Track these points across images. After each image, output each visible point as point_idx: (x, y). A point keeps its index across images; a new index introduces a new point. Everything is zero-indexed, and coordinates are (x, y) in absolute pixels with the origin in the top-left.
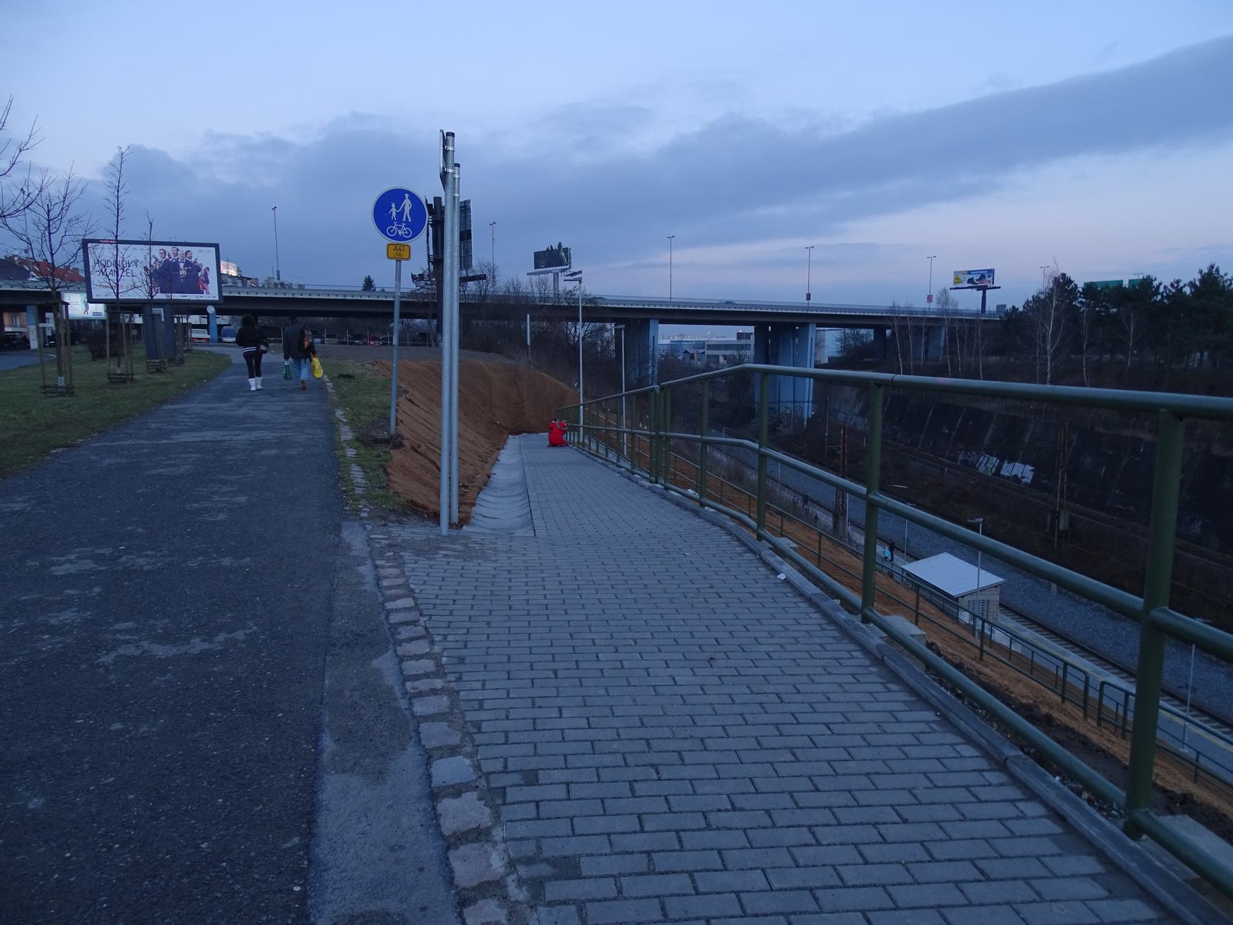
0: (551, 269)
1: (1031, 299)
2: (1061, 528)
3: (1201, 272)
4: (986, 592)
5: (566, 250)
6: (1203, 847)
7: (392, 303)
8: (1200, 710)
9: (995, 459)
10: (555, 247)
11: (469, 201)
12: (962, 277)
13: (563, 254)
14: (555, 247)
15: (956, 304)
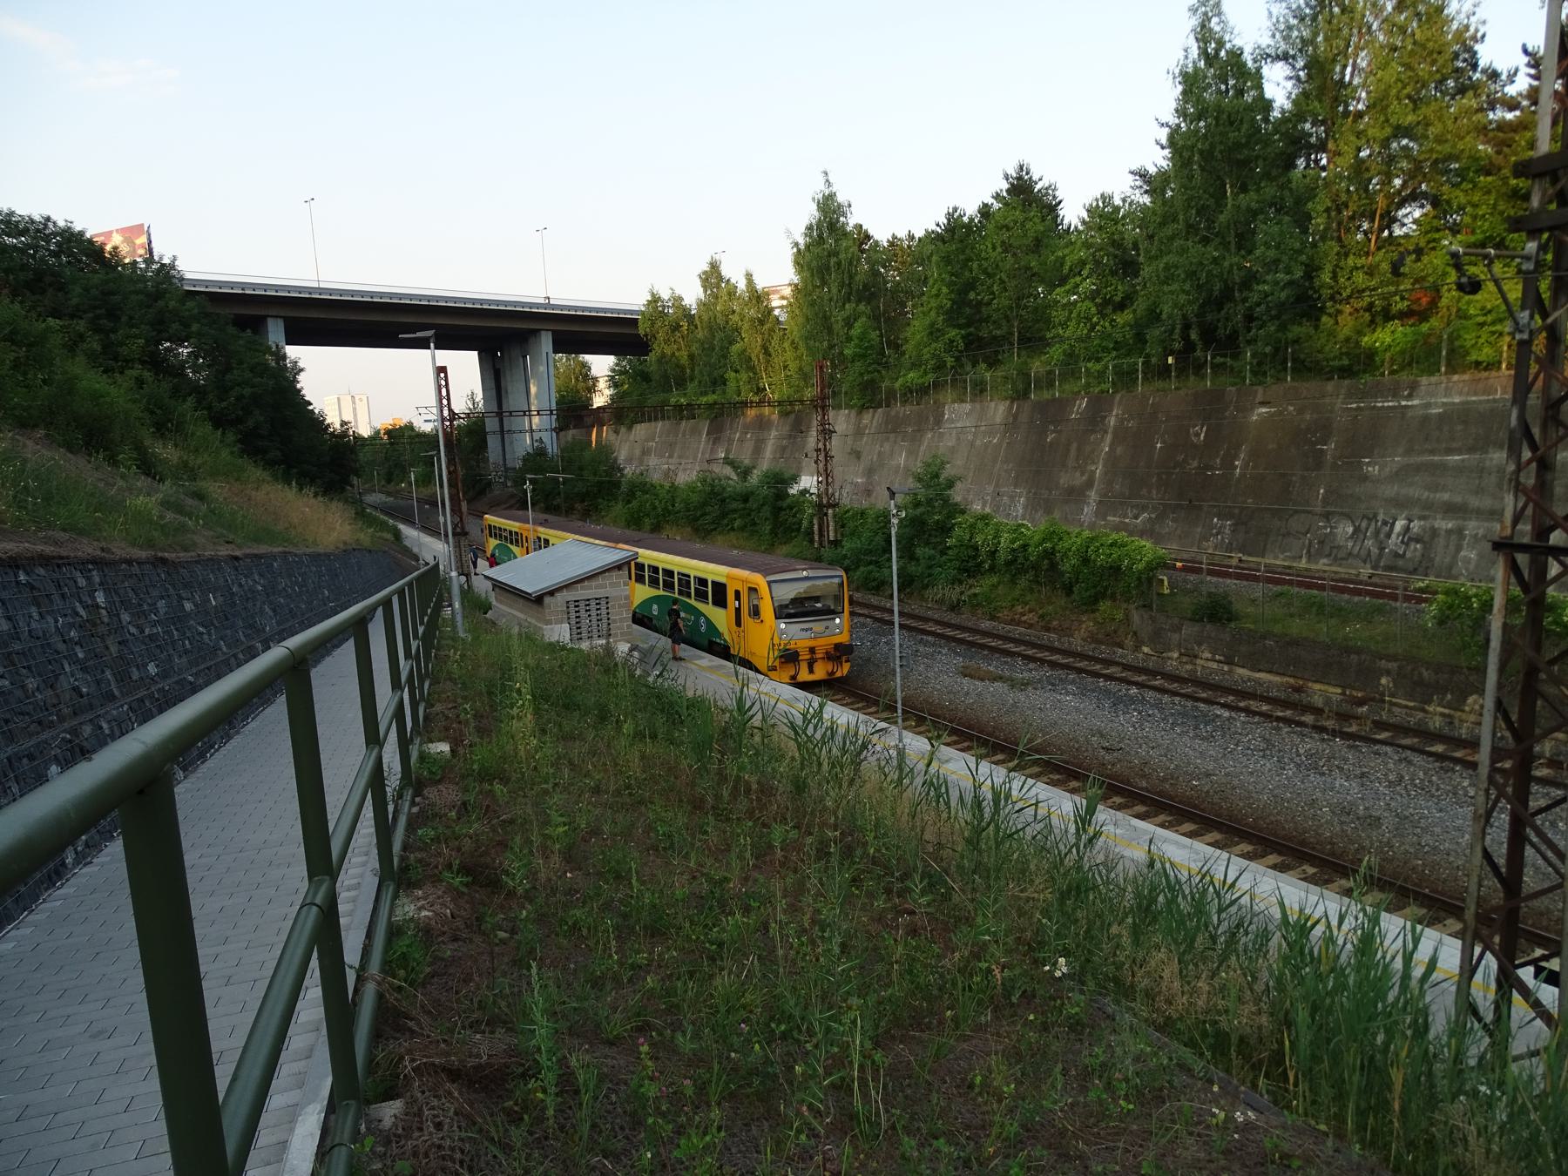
4: (600, 580)
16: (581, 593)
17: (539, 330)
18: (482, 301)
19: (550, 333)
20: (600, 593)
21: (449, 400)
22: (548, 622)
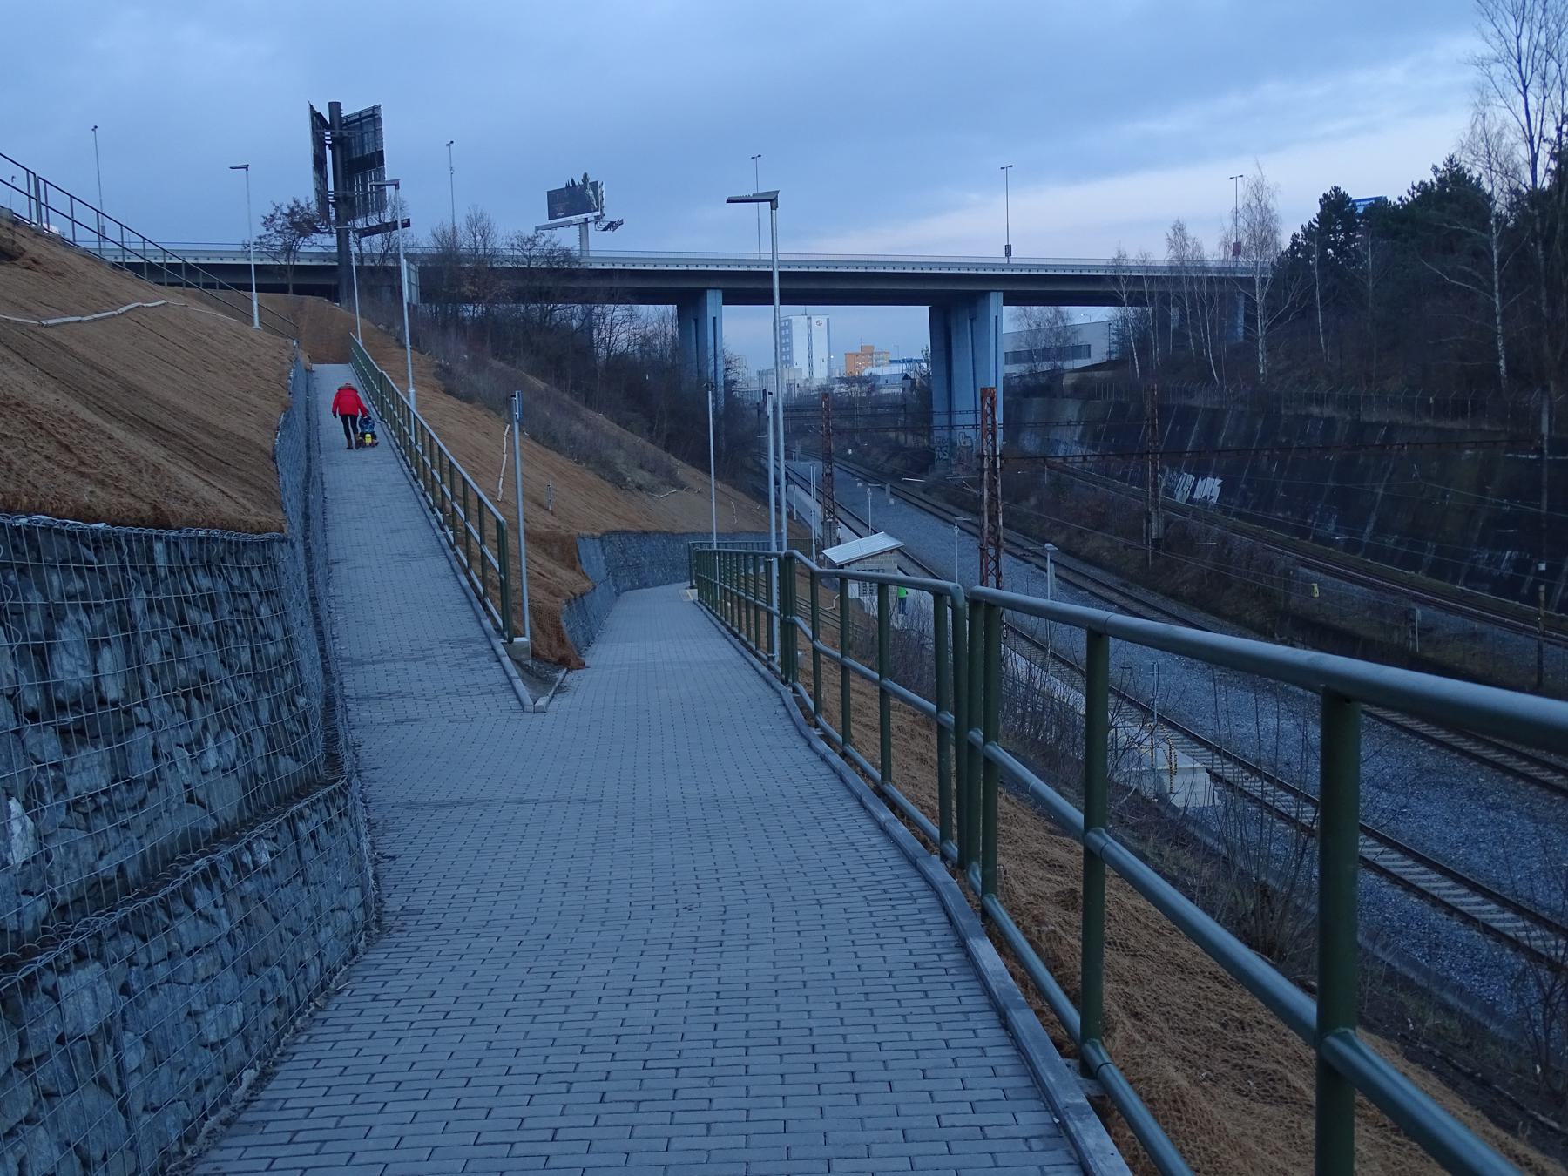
0: (573, 218)
1: (1300, 232)
2: (1154, 534)
3: (1435, 169)
5: (595, 186)
7: (770, 274)
10: (579, 181)
11: (377, 108)
13: (591, 192)
14: (579, 181)
15: (1199, 248)
19: (1001, 294)
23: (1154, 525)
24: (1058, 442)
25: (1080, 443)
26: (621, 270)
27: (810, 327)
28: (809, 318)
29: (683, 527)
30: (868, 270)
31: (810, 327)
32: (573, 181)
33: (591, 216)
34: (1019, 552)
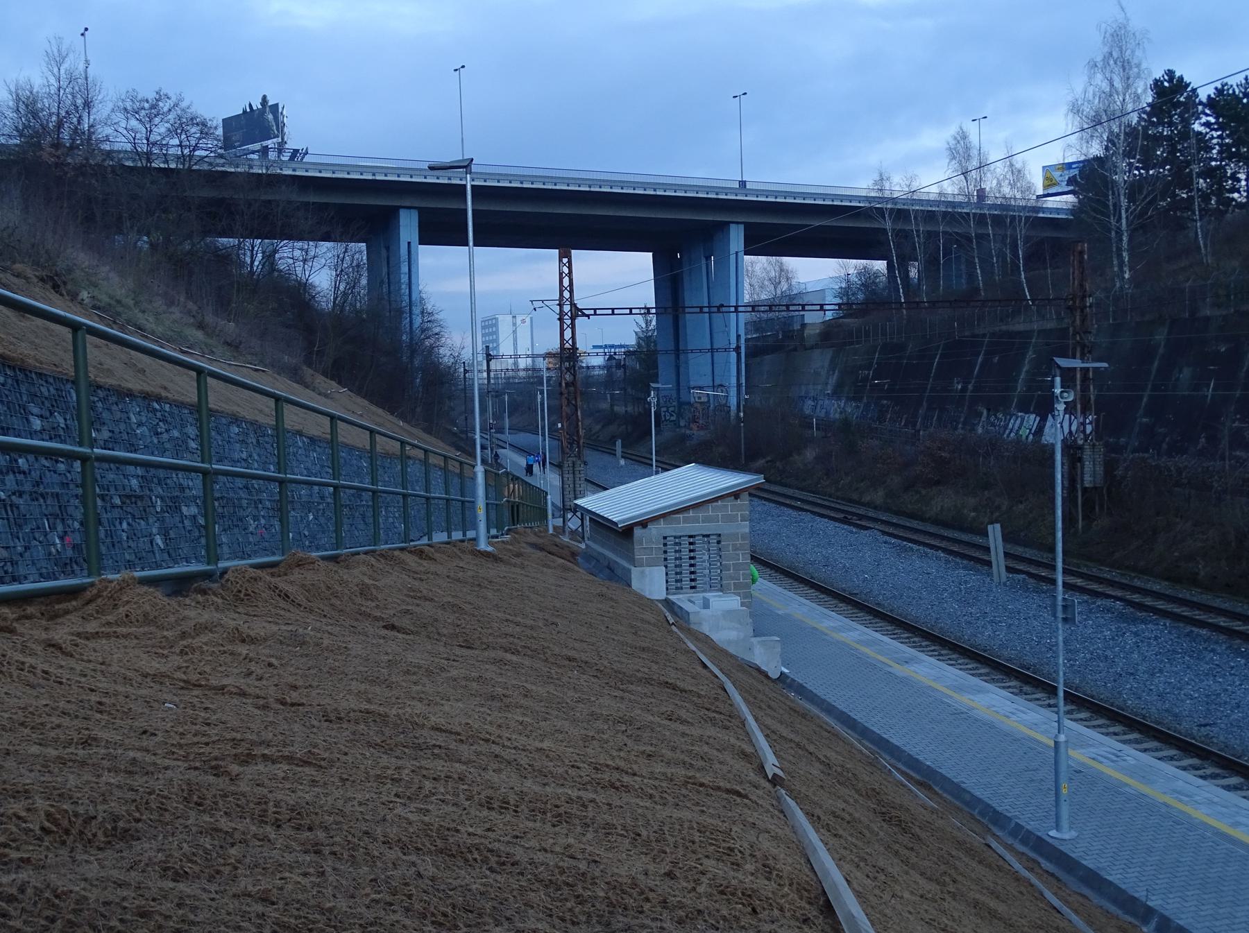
2: (1088, 481)
4: (710, 511)
5: (275, 108)
6: (1169, 769)
8: (1081, 703)
9: (1033, 416)
10: (257, 105)
12: (1057, 174)
13: (270, 117)
14: (257, 105)
16: (682, 527)
17: (728, 223)
18: (776, 193)
19: (742, 227)
20: (710, 528)
21: (571, 292)
22: (632, 561)
23: (1088, 465)
24: (803, 399)
25: (836, 394)
26: (291, 176)
27: (514, 324)
28: (514, 317)
29: (109, 372)
30: (592, 189)
31: (514, 324)
32: (250, 105)
33: (270, 143)
34: (841, 516)
